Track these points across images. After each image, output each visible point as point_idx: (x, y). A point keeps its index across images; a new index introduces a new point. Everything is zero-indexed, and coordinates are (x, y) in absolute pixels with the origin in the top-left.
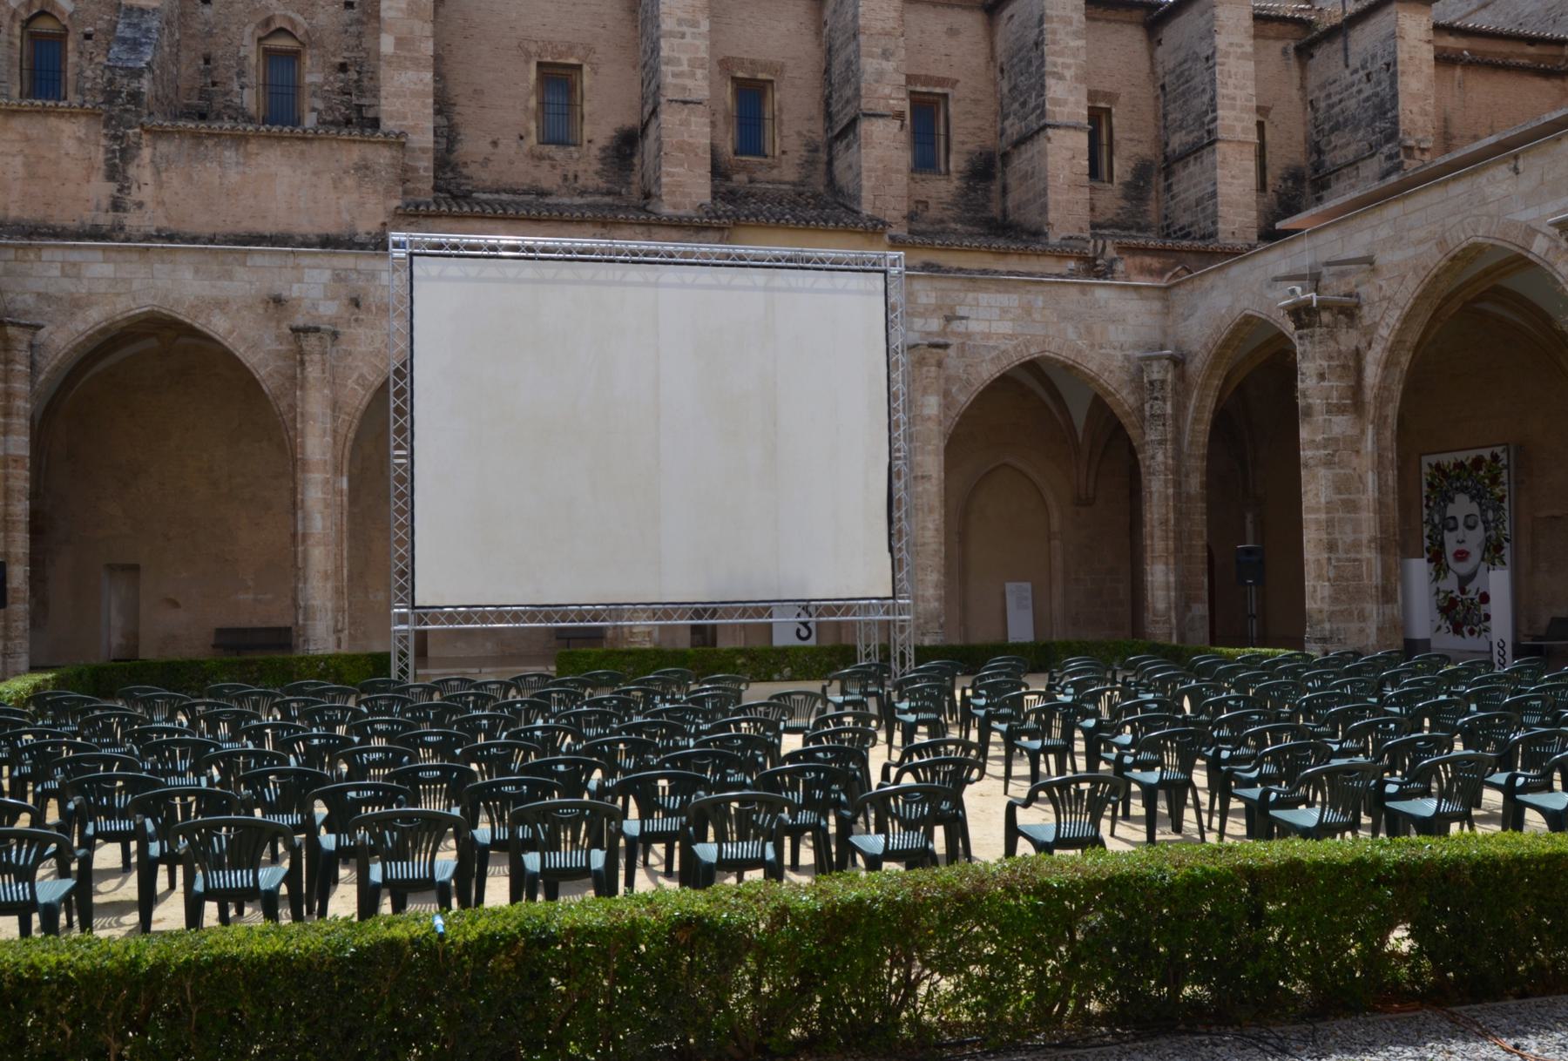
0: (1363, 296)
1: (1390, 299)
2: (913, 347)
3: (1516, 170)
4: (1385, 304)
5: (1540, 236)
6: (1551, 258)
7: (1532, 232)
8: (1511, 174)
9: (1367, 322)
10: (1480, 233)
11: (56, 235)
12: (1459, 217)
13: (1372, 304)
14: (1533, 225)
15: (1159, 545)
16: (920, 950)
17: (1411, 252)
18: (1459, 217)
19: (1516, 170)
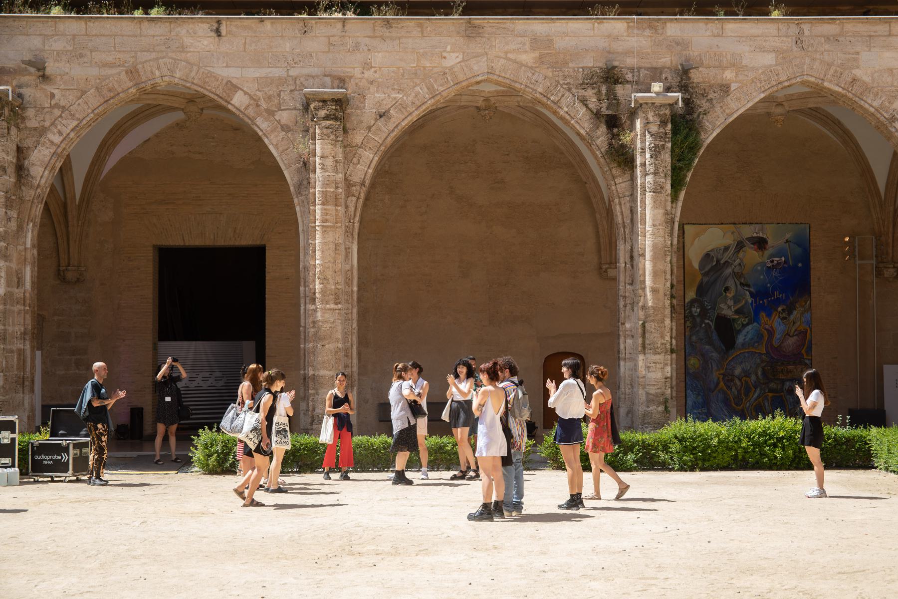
0: (27, 98)
1: (63, 109)
2: (444, 459)
3: (218, 32)
4: (57, 112)
5: (240, 93)
6: (251, 112)
7: (233, 87)
8: (213, 34)
9: (33, 123)
10: (178, 75)
11: (692, 483)
12: (153, 55)
13: (40, 110)
14: (234, 81)
15: (648, 265)
16: (444, 51)
17: (95, 71)
18: (153, 55)
19: (218, 32)
